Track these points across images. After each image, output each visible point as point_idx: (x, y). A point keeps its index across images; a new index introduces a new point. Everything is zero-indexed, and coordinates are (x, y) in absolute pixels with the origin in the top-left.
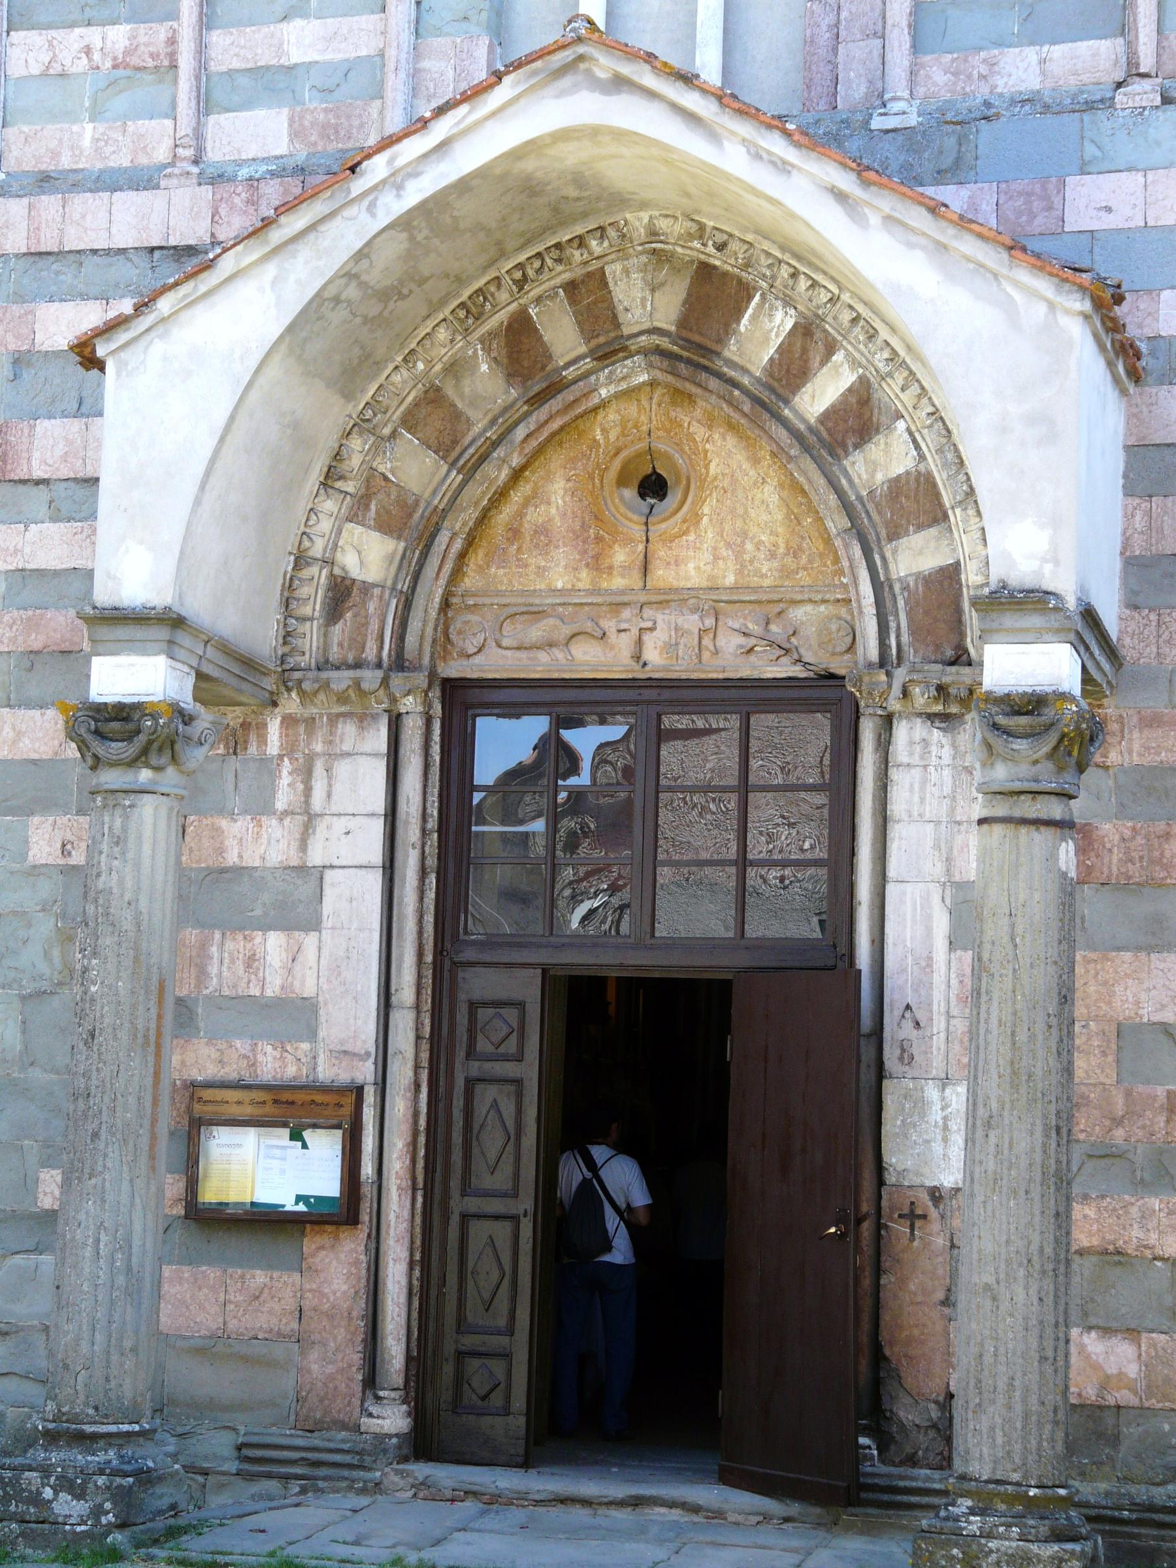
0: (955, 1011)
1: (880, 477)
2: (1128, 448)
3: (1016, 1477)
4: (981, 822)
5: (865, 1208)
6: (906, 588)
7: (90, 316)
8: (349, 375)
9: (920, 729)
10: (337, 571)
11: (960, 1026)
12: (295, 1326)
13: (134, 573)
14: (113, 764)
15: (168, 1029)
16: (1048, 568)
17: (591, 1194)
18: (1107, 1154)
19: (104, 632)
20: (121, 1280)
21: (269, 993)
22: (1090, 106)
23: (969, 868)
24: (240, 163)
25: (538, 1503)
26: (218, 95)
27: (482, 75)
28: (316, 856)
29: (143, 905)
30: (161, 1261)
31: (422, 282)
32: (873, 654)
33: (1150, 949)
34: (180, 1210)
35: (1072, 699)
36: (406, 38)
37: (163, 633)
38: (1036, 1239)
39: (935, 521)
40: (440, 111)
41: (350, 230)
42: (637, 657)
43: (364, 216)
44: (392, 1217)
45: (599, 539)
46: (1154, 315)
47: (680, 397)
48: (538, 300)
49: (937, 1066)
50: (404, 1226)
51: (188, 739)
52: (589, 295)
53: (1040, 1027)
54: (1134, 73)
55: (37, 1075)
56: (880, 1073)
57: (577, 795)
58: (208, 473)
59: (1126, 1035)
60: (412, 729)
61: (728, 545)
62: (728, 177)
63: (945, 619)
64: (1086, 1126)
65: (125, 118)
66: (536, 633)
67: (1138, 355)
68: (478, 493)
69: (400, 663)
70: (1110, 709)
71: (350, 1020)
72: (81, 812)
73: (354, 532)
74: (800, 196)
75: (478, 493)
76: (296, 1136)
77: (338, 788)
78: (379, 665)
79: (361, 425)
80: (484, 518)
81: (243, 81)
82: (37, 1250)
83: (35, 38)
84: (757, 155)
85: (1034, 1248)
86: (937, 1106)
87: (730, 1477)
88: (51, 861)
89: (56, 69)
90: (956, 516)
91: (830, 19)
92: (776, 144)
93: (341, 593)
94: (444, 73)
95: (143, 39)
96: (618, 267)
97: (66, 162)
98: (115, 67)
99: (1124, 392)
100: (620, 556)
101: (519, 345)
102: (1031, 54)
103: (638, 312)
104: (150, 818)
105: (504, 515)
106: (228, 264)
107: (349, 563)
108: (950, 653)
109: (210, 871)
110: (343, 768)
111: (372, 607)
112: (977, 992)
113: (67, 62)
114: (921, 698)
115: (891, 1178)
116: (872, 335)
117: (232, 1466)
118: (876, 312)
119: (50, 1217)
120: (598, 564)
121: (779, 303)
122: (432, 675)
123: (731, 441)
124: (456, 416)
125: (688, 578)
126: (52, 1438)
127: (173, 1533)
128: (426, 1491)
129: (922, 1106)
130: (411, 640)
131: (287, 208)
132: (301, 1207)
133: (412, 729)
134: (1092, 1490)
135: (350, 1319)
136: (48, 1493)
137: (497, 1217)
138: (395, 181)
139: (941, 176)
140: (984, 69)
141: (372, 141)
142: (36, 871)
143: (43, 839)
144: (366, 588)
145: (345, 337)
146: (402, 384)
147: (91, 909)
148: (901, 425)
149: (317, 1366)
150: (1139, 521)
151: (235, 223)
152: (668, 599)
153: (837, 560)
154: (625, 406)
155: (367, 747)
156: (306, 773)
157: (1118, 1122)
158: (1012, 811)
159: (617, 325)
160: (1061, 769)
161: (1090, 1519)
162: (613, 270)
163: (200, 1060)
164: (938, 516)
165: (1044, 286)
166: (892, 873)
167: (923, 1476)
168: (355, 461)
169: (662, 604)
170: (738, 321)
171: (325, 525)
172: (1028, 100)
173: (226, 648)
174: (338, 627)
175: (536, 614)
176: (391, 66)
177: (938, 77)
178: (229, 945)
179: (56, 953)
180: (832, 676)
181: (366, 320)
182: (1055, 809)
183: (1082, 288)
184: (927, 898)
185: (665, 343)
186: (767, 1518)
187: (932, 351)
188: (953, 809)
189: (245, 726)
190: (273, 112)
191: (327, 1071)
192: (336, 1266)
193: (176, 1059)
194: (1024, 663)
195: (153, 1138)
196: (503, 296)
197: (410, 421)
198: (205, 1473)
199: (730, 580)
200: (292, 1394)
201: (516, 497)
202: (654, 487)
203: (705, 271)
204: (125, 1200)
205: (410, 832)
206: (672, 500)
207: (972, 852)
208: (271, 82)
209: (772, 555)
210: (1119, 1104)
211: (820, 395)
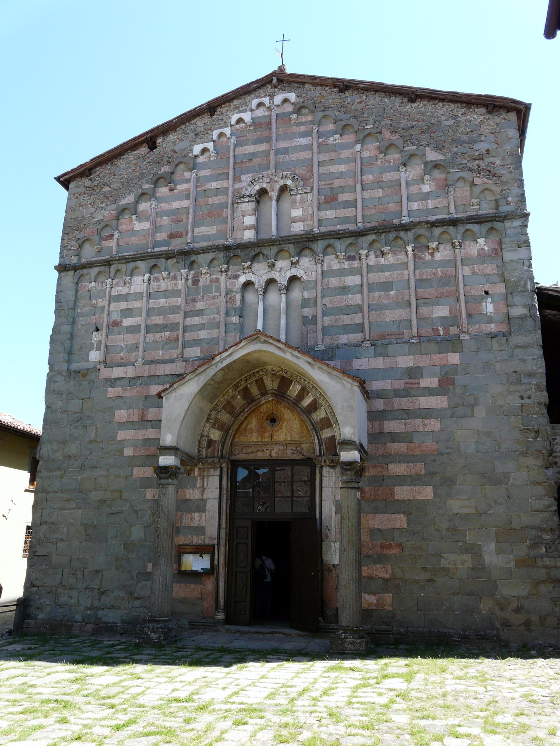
1: (319, 418)
2: (368, 412)
3: (351, 625)
4: (341, 488)
5: (319, 569)
6: (324, 440)
7: (160, 388)
8: (212, 399)
9: (328, 469)
11: (338, 530)
13: (168, 439)
14: (164, 478)
15: (174, 534)
16: (353, 436)
17: (263, 567)
18: (369, 556)
19: (162, 451)
20: (164, 587)
21: (195, 525)
22: (357, 346)
23: (339, 497)
24: (190, 358)
25: (252, 633)
26: (186, 345)
27: (238, 340)
28: (205, 497)
29: (169, 508)
30: (173, 583)
31: (227, 380)
32: (318, 454)
33: (376, 513)
34: (176, 572)
35: (358, 463)
36: (223, 334)
37: (174, 451)
38: (354, 575)
39: (330, 427)
40: (230, 347)
41: (212, 371)
42: (270, 455)
43: (215, 368)
45: (262, 431)
46: (371, 386)
47: (278, 402)
48: (250, 384)
49: (333, 539)
50: (223, 574)
51: (179, 473)
52: (260, 383)
53: (354, 530)
54: (365, 340)
55: (148, 543)
56: (322, 540)
57: (258, 483)
58: (183, 419)
59: (372, 531)
60: (225, 470)
62: (287, 359)
63: (333, 446)
64: (364, 551)
66: (250, 450)
67: (369, 394)
68: (238, 422)
69: (222, 457)
70: (366, 464)
71: (212, 531)
72: (157, 488)
73: (213, 430)
74: (302, 363)
75: (238, 422)
76: (201, 556)
77: (210, 482)
78: (218, 457)
79: (214, 409)
80: (239, 427)
81: (191, 342)
82: (147, 580)
83: (151, 335)
84: (293, 355)
85: (354, 577)
86: (333, 547)
87: (292, 627)
90: (334, 426)
91: (307, 329)
92: (296, 353)
93: (210, 443)
94: (231, 340)
96: (265, 377)
97: (156, 358)
99: (366, 401)
100: (267, 434)
101: (246, 393)
102: (345, 336)
104: (171, 489)
105: (243, 426)
106: (188, 378)
107: (212, 436)
108: (334, 453)
109: (183, 500)
110: (210, 478)
112: (341, 523)
114: (328, 462)
115: (324, 562)
116: (316, 390)
117: (188, 626)
118: (317, 385)
119: (150, 573)
120: (262, 436)
122: (229, 459)
123: (289, 411)
124: (233, 407)
126: (150, 621)
127: (176, 641)
128: (228, 631)
129: (330, 547)
130: (224, 452)
131: (199, 366)
132: (202, 571)
133: (225, 470)
134: (367, 627)
136: (149, 633)
137: (243, 572)
138: (221, 361)
139: (329, 359)
141: (217, 353)
143: (149, 494)
144: (215, 441)
145: (210, 392)
146: (222, 400)
147: (159, 509)
148: (323, 408)
149: (205, 605)
150: (370, 426)
151: (189, 369)
152: (277, 443)
153: (310, 435)
154: (267, 404)
156: (203, 480)
157: (370, 549)
158: (347, 486)
160: (357, 477)
161: (366, 633)
163: (181, 540)
164: (330, 426)
165: (350, 380)
167: (332, 626)
168: (213, 416)
169: (275, 444)
171: (207, 429)
172: (346, 345)
173: (187, 454)
175: (249, 446)
176: (220, 338)
177: (328, 340)
178: (187, 516)
179: (151, 517)
180: (310, 458)
181: (215, 388)
182: (356, 485)
183: (357, 381)
184: (330, 504)
185: (275, 392)
186: (300, 635)
187: (329, 393)
189: (191, 470)
191: (207, 542)
192: (209, 584)
193: (176, 540)
194: (349, 455)
195: (171, 556)
197: (224, 408)
198: (182, 628)
199: (289, 439)
201: (245, 423)
202: (273, 420)
203: (283, 378)
204: (165, 570)
205: (224, 491)
206: (277, 423)
207: (339, 494)
208: (197, 342)
209: (297, 434)
210: (370, 546)
211: (307, 402)
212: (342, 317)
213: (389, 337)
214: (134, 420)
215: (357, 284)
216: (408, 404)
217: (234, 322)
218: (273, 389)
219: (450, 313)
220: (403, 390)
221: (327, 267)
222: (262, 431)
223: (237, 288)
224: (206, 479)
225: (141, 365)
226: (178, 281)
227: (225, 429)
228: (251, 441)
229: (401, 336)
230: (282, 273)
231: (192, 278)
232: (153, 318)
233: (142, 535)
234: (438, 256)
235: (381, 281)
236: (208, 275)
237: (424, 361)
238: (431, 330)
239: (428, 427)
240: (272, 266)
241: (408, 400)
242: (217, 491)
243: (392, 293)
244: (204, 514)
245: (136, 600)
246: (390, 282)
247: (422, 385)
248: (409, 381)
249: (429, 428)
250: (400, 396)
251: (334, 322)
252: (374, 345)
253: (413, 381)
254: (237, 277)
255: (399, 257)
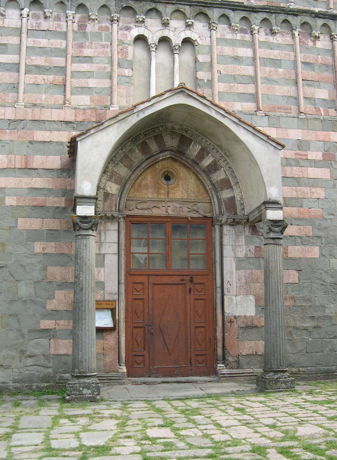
0: (237, 282)
1: (219, 179)
10: (105, 191)
12: (102, 351)
28: (103, 252)
39: (230, 188)
44: (122, 327)
61: (185, 190)
65: (53, 94)
66: (145, 206)
73: (109, 183)
86: (235, 301)
88: (40, 252)
89: (36, 83)
90: (234, 187)
95: (57, 79)
96: (165, 134)
98: (50, 84)
102: (240, 104)
103: (169, 143)
110: (108, 232)
111: (114, 199)
113: (39, 82)
120: (158, 193)
121: (198, 144)
124: (131, 161)
125: (177, 196)
130: (121, 206)
135: (115, 349)
140: (231, 105)
142: (36, 254)
144: (112, 195)
148: (222, 169)
155: (113, 228)
159: (165, 145)
162: (164, 134)
166: (224, 255)
170: (190, 146)
174: (106, 203)
188: (235, 243)
190: (86, 96)
191: (107, 298)
192: (111, 339)
196: (141, 137)
199: (186, 197)
200: (103, 366)
201: (140, 178)
203: (182, 136)
209: (194, 193)
212: (236, 85)
213: (279, 110)
214: (17, 167)
215: (249, 56)
216: (298, 173)
217: (127, 75)
218: (172, 147)
219: (329, 97)
220: (294, 160)
221: (221, 35)
222: (158, 188)
223: (129, 41)
224: (103, 233)
225: (23, 107)
226: (62, 23)
227: (123, 184)
228: (146, 197)
229: (289, 111)
230: (177, 33)
231: (79, 21)
232: (34, 58)
233: (32, 291)
234: (319, 44)
235: (271, 57)
236: (96, 22)
237: (310, 136)
238: (314, 109)
239: (315, 194)
240: (165, 24)
241: (298, 169)
242: (116, 246)
243: (281, 70)
244: (102, 269)
245: (29, 359)
246: (279, 60)
247: (309, 158)
248: (298, 152)
249: (316, 196)
250: (291, 165)
251: (228, 89)
252: (268, 116)
253: (302, 152)
254: (128, 29)
255: (286, 38)
